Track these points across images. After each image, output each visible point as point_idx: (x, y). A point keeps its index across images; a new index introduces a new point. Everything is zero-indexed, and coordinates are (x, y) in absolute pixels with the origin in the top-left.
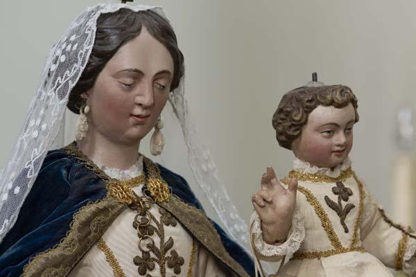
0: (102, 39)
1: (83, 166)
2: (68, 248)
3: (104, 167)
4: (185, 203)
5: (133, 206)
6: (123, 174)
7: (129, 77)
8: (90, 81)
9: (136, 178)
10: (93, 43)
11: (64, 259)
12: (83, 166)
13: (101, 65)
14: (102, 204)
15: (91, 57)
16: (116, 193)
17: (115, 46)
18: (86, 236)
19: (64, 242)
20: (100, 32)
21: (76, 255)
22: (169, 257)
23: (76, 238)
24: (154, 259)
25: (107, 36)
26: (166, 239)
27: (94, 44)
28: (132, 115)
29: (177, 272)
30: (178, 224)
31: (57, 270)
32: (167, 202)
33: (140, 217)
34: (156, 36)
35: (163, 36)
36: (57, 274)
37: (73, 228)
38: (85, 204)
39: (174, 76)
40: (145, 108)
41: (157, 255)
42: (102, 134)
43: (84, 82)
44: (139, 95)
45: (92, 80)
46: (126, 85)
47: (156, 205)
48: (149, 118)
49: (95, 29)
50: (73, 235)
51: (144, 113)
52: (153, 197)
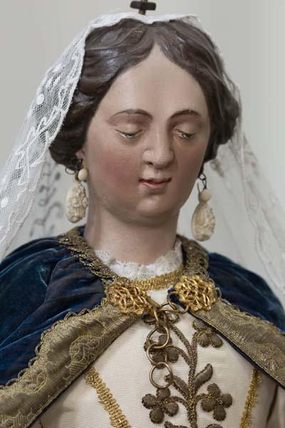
0: (92, 66)
1: (77, 260)
2: (32, 385)
3: (113, 262)
4: (241, 311)
5: (146, 318)
6: (145, 270)
7: (129, 121)
8: (78, 131)
9: (165, 276)
10: (80, 72)
11: (23, 401)
12: (77, 260)
13: (92, 106)
14: (90, 317)
15: (76, 93)
16: (118, 299)
17: (109, 76)
18: (62, 366)
19: (24, 376)
20: (89, 57)
21: (43, 398)
22: (204, 395)
23: (45, 369)
24: (176, 399)
25: (100, 61)
26: (200, 367)
28: (142, 180)
29: (220, 417)
30: (226, 344)
31: (10, 418)
32: (206, 310)
33: (157, 334)
34: (175, 59)
35: (188, 58)
36: (11, 425)
37: (40, 354)
38: (62, 317)
39: (220, 117)
40: (159, 168)
41: (182, 392)
42: (109, 210)
43: (71, 133)
45: (81, 129)
46: (126, 134)
47: (188, 316)
48: (170, 184)
49: (82, 53)
50: (40, 364)
51: (158, 176)
52: (183, 305)
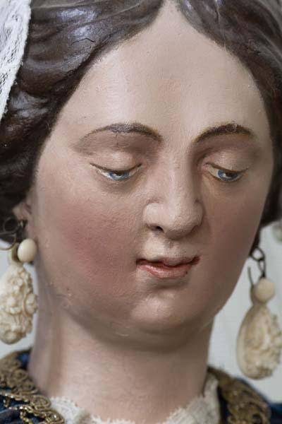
7: (117, 147)
13: (45, 117)
17: (78, 60)
25: (59, 30)
27: (25, 58)
28: (141, 261)
34: (207, 27)
40: (175, 237)
44: (154, 200)
45: (24, 162)
46: (112, 172)
48: (196, 269)
